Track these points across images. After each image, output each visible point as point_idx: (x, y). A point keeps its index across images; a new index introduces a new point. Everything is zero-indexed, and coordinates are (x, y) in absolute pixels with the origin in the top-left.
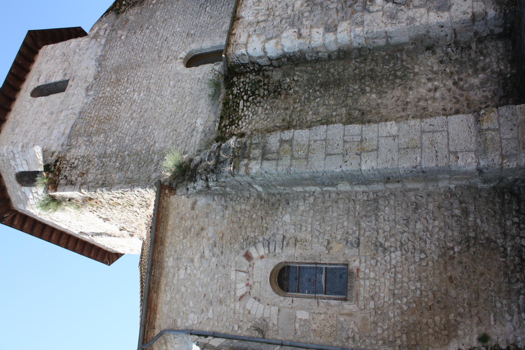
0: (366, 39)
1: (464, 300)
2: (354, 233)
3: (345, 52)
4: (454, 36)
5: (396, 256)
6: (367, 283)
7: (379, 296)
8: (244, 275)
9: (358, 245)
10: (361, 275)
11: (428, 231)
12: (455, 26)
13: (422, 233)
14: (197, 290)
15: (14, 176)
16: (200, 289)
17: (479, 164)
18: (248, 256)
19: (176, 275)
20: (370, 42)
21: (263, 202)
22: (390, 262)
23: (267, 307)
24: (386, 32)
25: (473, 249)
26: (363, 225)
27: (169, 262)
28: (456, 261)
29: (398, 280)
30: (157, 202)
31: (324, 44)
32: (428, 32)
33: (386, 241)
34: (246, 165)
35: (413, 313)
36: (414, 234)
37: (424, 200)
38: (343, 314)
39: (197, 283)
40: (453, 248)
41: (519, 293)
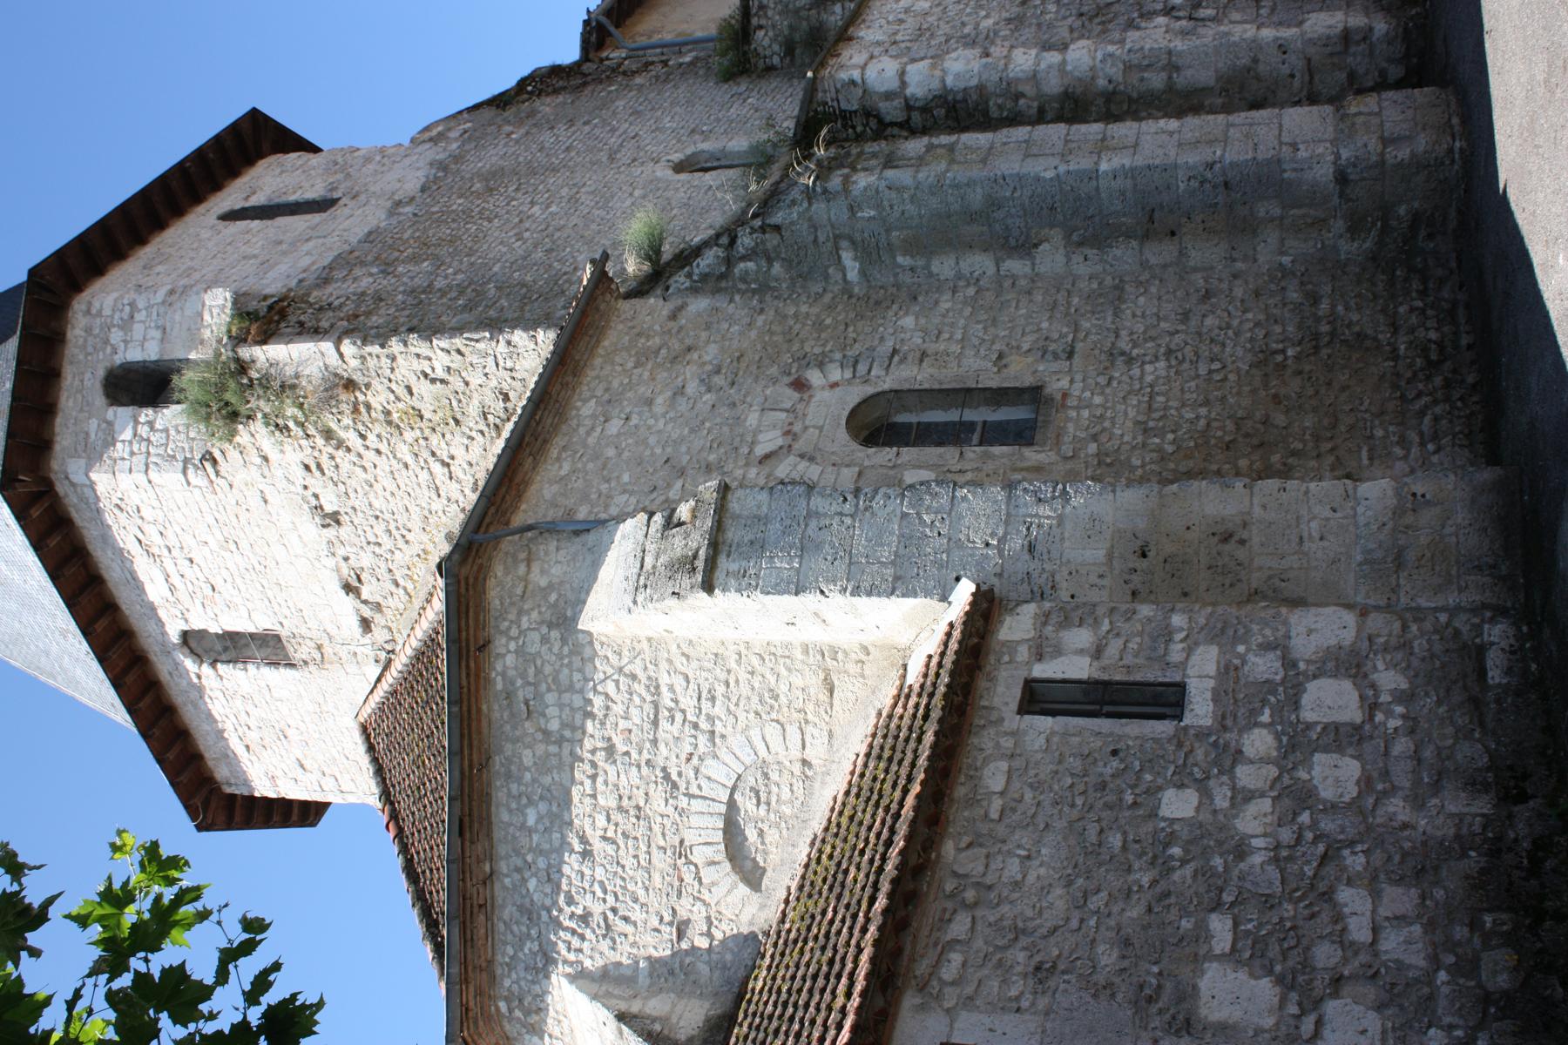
0: (1128, 67)
1: (1305, 429)
2: (1066, 336)
3: (1076, 102)
4: (1307, 78)
5: (1156, 370)
6: (1086, 413)
8: (784, 415)
9: (1070, 355)
10: (1071, 402)
11: (1229, 327)
12: (1311, 51)
13: (1217, 331)
14: (648, 452)
15: (101, 373)
16: (658, 451)
17: (1338, 156)
18: (800, 385)
19: (599, 430)
20: (1134, 78)
21: (854, 300)
23: (830, 469)
24: (1170, 53)
25: (1325, 352)
26: (1086, 325)
27: (585, 409)
28: (1289, 372)
29: (1155, 406)
30: (504, 460)
31: (1035, 73)
32: (1255, 61)
33: (1134, 347)
34: (846, 178)
35: (1187, 457)
36: (1199, 334)
39: (652, 440)
40: (1283, 351)
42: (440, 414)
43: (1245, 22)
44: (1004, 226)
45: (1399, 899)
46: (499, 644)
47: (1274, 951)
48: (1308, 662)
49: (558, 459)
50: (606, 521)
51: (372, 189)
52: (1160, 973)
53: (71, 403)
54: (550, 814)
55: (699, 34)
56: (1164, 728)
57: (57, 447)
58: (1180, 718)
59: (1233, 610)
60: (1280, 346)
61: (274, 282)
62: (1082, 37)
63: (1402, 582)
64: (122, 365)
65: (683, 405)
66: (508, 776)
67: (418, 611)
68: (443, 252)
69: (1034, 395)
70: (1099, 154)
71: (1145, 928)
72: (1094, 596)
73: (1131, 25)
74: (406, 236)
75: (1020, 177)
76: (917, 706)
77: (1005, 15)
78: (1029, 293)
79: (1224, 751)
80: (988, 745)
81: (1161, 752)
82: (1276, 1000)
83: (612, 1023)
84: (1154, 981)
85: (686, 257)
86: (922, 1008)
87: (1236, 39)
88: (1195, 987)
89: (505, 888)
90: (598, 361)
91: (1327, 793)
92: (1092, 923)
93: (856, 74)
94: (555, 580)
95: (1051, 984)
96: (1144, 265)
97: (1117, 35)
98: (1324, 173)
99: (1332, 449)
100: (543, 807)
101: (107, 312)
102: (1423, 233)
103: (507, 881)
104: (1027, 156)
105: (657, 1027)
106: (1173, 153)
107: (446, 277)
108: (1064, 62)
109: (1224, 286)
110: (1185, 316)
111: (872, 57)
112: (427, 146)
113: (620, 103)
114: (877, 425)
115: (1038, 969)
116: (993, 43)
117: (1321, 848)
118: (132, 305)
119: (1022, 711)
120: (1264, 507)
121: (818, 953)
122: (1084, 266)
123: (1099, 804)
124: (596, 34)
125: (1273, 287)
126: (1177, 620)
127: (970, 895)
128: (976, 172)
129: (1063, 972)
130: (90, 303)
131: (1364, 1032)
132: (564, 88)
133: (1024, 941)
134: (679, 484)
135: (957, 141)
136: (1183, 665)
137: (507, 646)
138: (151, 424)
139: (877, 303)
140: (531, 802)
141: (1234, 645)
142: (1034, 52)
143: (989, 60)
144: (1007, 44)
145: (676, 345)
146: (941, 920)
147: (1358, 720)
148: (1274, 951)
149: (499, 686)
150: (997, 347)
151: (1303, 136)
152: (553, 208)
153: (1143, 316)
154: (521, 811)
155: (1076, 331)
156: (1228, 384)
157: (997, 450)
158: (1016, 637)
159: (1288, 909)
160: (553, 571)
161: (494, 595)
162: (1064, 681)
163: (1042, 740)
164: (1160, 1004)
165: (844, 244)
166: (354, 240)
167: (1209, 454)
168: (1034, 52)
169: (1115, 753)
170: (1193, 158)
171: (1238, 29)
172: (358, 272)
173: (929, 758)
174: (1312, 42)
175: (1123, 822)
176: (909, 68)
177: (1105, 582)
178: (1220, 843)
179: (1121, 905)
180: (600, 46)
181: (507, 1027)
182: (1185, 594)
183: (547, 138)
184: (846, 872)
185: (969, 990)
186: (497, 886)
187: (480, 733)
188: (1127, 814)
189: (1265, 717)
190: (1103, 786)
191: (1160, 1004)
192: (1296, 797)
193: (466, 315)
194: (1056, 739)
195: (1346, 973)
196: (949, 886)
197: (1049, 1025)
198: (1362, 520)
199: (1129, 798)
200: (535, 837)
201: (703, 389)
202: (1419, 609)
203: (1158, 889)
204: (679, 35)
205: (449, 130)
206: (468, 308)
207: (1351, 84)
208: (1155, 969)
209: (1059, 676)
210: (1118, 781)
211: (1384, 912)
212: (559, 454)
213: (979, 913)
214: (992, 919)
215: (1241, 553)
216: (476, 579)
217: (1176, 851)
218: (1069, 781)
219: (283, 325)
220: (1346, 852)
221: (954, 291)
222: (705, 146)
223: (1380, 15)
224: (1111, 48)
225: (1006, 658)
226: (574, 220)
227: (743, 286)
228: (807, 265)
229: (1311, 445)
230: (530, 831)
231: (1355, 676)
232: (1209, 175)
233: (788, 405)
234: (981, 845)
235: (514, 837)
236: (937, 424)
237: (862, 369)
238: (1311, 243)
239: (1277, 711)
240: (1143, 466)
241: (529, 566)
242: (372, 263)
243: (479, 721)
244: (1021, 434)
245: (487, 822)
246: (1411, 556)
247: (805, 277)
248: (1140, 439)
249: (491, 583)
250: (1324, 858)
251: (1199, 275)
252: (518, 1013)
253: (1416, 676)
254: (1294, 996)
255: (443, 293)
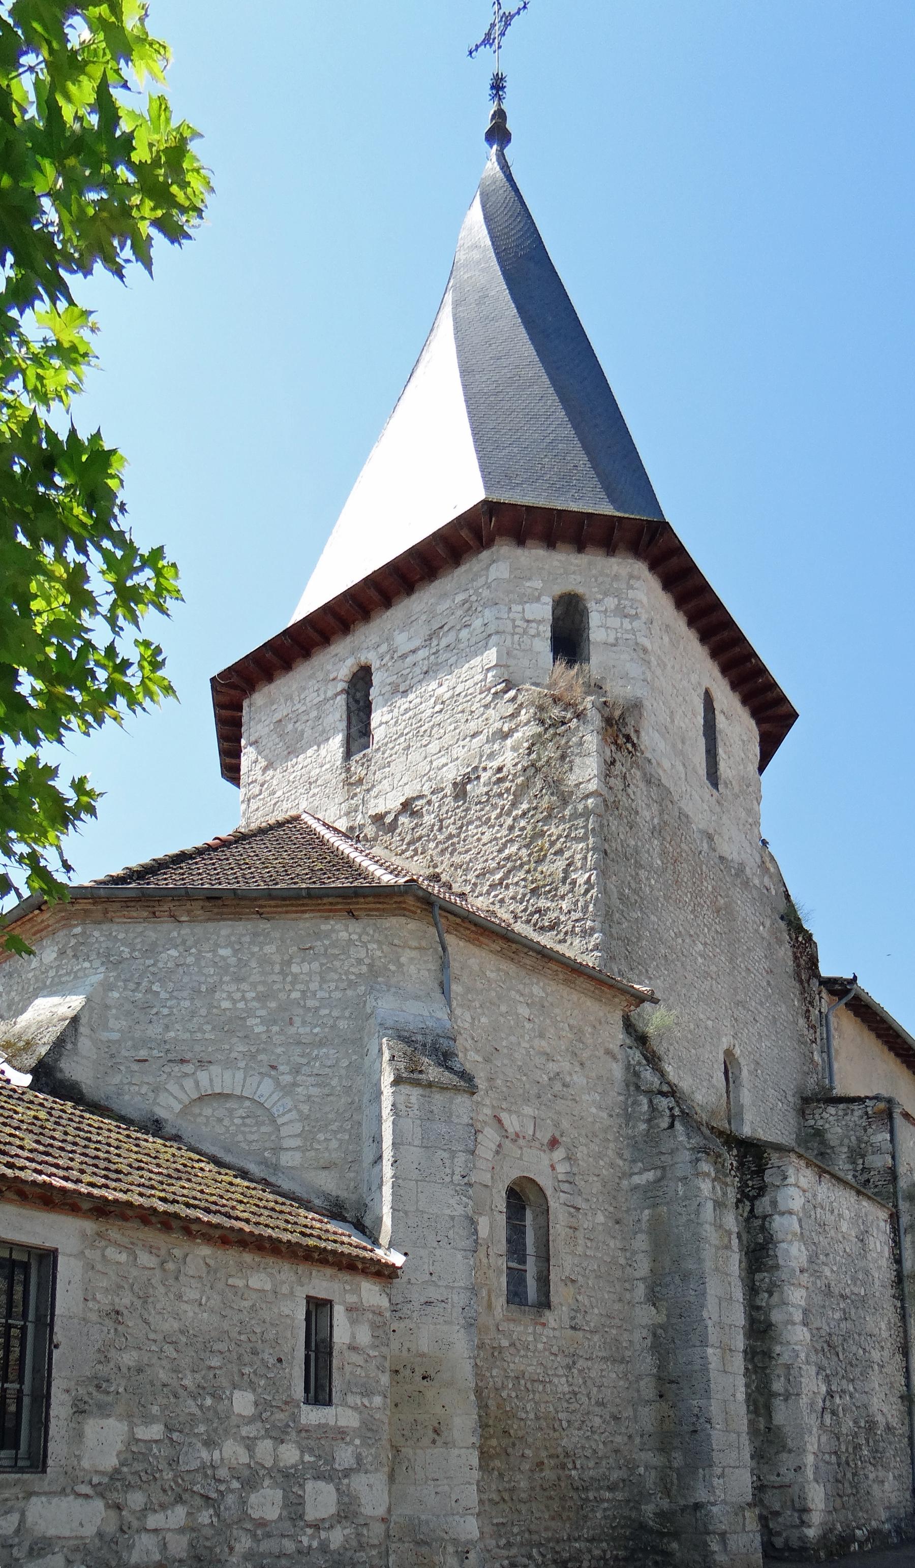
0: (788, 1367)
3: (765, 1331)
4: (776, 1485)
6: (531, 1338)
7: (515, 1356)
9: (573, 1328)
10: (539, 1329)
12: (796, 1488)
14: (503, 1035)
15: (580, 590)
16: (504, 1043)
18: (554, 1143)
19: (521, 999)
20: (780, 1371)
21: (617, 1180)
22: (556, 1375)
23: (491, 1166)
24: (798, 1395)
26: (596, 1338)
28: (560, 1472)
29: (536, 1384)
32: (790, 1451)
36: (588, 1413)
37: (623, 1430)
38: (489, 1296)
39: (513, 1039)
40: (575, 1468)
41: (530, 1557)
42: (540, 877)
43: (819, 1445)
44: (669, 1281)
45: (179, 1546)
46: (355, 927)
47: (137, 1466)
48: (349, 1485)
49: (499, 970)
50: (450, 1007)
51: (724, 817)
52: (118, 1393)
53: (556, 563)
54: (228, 966)
55: (836, 1066)
56: (299, 1392)
57: (519, 551)
58: (307, 1402)
59: (385, 1436)
60: (578, 1466)
61: (651, 740)
62: (813, 1336)
63: (406, 1545)
64: (586, 608)
65: (539, 1060)
66: (255, 935)
67: (380, 867)
68: (669, 875)
69: (545, 1303)
70: (720, 1347)
71: (152, 1384)
72: (395, 1345)
73: (821, 1368)
74: (683, 845)
75: (704, 1294)
76: (312, 1228)
77: (833, 1284)
78: (620, 1300)
79: (283, 1432)
80: (283, 1276)
81: (281, 1391)
82: (101, 1468)
83: (71, 1013)
84: (112, 1389)
85: (653, 1060)
86: (84, 1235)
87: (806, 1438)
88: (109, 1416)
89: (170, 932)
90: (575, 996)
91: (253, 1498)
92: (154, 1348)
93: (791, 1180)
94: (405, 969)
95: (107, 1321)
96: (639, 1377)
97: (813, 1358)
98: (702, 1495)
99: (504, 1500)
100: (233, 961)
101: (631, 594)
102: (659, 1558)
103: (175, 934)
104: (720, 1299)
105: (69, 1046)
106: (719, 1396)
107: (648, 879)
108: (794, 1324)
109: (623, 1430)
110: (601, 1404)
111: (804, 1191)
112: (758, 860)
113: (784, 1009)
114: (521, 1198)
115: (118, 1313)
116: (812, 1275)
117: (214, 1495)
118: (636, 616)
119: (309, 1299)
120: (459, 1456)
121: (126, 1161)
122: (639, 1338)
123: (242, 1351)
124: (841, 989)
125: (622, 1462)
126: (378, 1400)
127: (170, 1266)
128: (709, 1265)
129: (116, 1329)
130: (638, 578)
131: (81, 1525)
132: (798, 966)
133: (138, 1303)
134: (480, 1059)
135: (733, 1251)
136: (345, 1404)
137: (354, 933)
138: (538, 634)
139: (614, 1198)
140: (235, 952)
141: (360, 1437)
142: (803, 1303)
143: (798, 1273)
144: (810, 1285)
145: (585, 1055)
146: (151, 1247)
147: (306, 1518)
148: (137, 1466)
149: (323, 927)
150: (580, 1279)
151: (729, 1480)
152: (700, 960)
153: (602, 1376)
154: (229, 945)
155: (591, 1332)
156: (551, 1432)
157: (504, 1279)
158: (363, 1293)
159: (168, 1475)
160: (412, 967)
161: (393, 922)
162: (331, 1326)
163: (287, 1311)
164: (95, 1393)
165: (659, 1173)
166: (682, 804)
167: (500, 1420)
168: (803, 1303)
169: (280, 1360)
170: (715, 1409)
171: (814, 1440)
172: (655, 807)
173: (270, 1237)
174: (802, 1489)
175: (229, 1366)
176: (795, 1217)
177: (405, 1353)
178: (215, 1430)
179: (168, 1366)
180: (832, 992)
181: (61, 933)
182: (396, 1405)
183: (759, 953)
184: (189, 1180)
185: (99, 1267)
186: (171, 926)
187: (287, 912)
188: (235, 1370)
189: (307, 1458)
190: (255, 1352)
191: (95, 1393)
192: (250, 1480)
193: (616, 895)
194: (289, 1321)
195: (124, 1513)
196: (177, 1252)
197: (76, 1321)
198: (450, 1519)
199: (246, 1370)
200: (209, 955)
201: (552, 1075)
202: (388, 1555)
203: (181, 1391)
204: (837, 1051)
205: (771, 877)
206: (622, 897)
207: (771, 1513)
208: (121, 1390)
209: (335, 1323)
210: (258, 1363)
211: (169, 1536)
212: (503, 970)
213: (158, 1272)
214: (153, 1281)
215: (426, 1441)
216: (404, 909)
217: (209, 1402)
218: (258, 1330)
219: (613, 748)
220: (211, 1511)
221: (623, 1250)
222: (745, 1073)
223: (821, 1532)
224: (803, 1356)
225: (348, 1287)
226: (690, 976)
227: (629, 1102)
228: (646, 1147)
229: (507, 1486)
230: (214, 951)
231: (338, 1515)
232: (701, 1421)
233: (538, 1135)
234: (208, 1272)
235: (209, 939)
236: (524, 1239)
237: (565, 1187)
238: (652, 1487)
239: (313, 1466)
240: (492, 1377)
241: (416, 948)
242: (661, 819)
243: (296, 912)
244: (516, 1294)
245: (221, 917)
246: (424, 1550)
247: (635, 1146)
248: (512, 1374)
249: (403, 920)
250: (208, 1498)
251: (631, 1413)
252: (73, 942)
253: (339, 1554)
254: (106, 1480)
255: (636, 877)
